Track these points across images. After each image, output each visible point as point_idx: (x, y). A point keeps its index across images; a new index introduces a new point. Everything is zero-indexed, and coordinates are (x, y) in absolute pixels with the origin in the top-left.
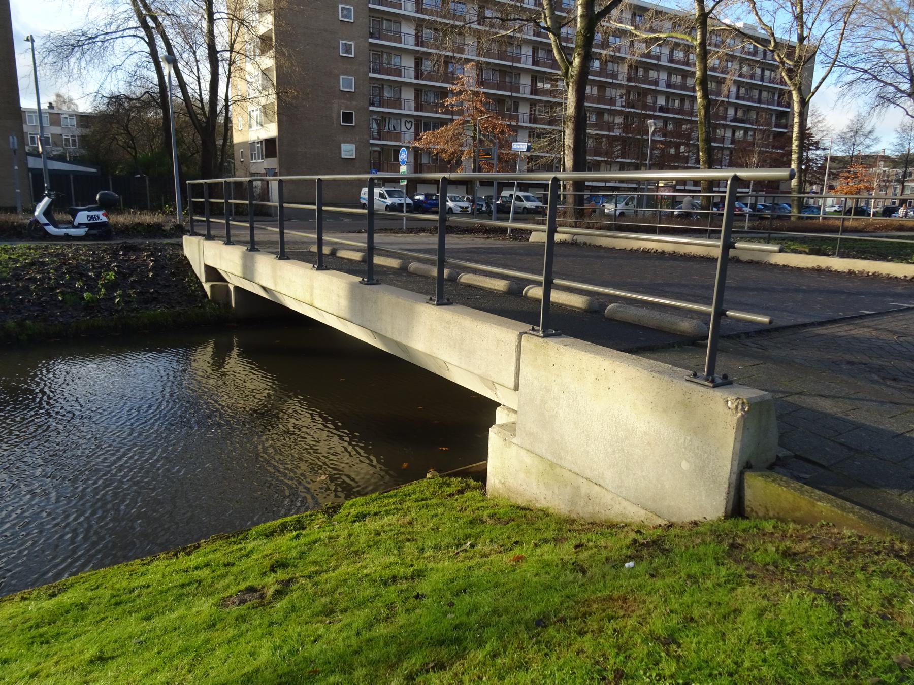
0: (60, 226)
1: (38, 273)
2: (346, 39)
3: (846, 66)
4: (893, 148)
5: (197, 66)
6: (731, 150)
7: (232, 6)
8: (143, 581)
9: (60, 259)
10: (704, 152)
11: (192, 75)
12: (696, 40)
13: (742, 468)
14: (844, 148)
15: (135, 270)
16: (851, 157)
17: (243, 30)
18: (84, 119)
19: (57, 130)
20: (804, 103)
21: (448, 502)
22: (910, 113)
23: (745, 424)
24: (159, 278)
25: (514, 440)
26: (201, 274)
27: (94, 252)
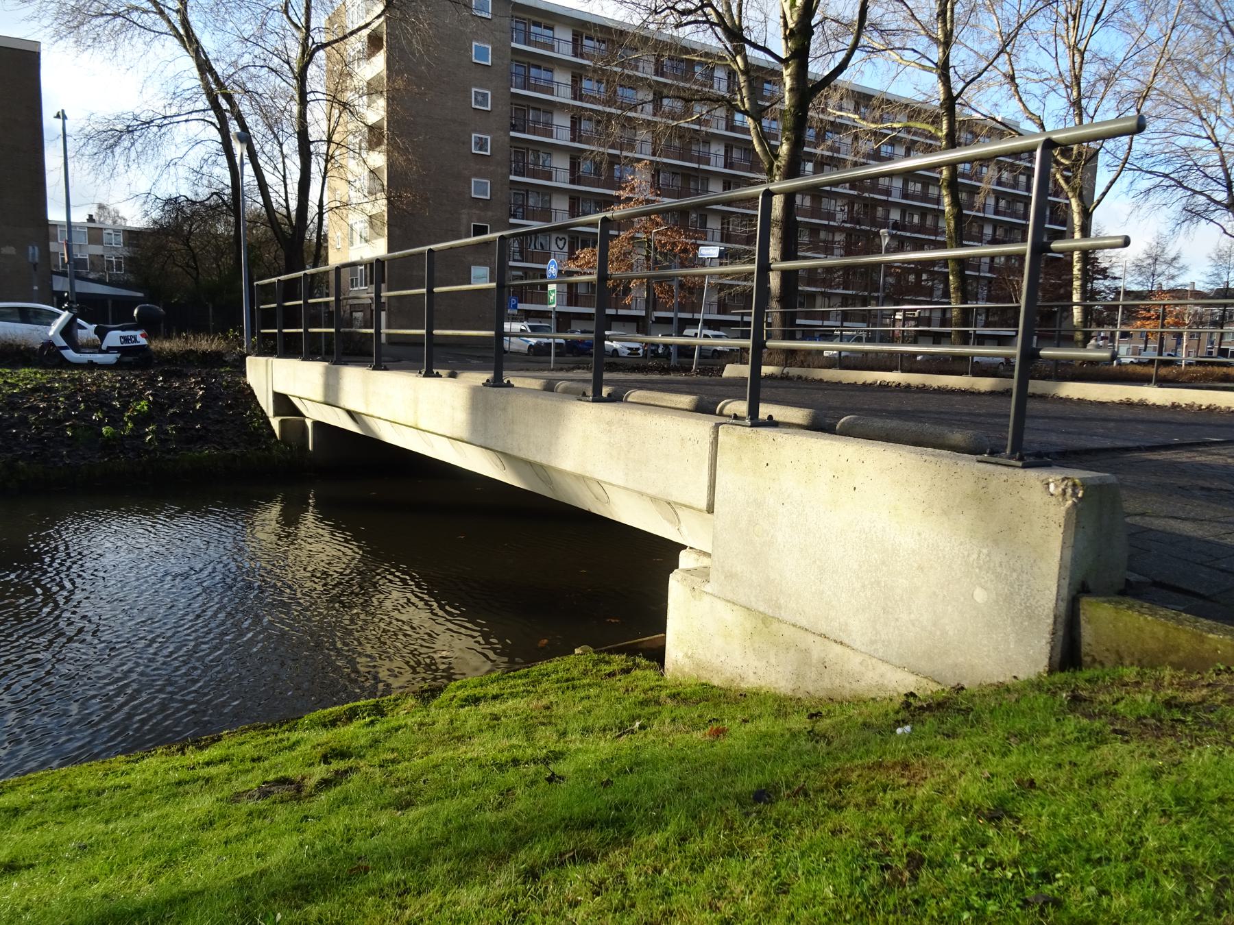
0: (83, 350)
1: (42, 400)
2: (480, 132)
3: (1140, 169)
4: (1207, 280)
5: (284, 162)
6: (990, 280)
7: (332, 87)
8: (122, 781)
9: (75, 385)
11: (277, 174)
12: (941, 131)
13: (1075, 593)
14: (1140, 279)
15: (178, 400)
17: (346, 116)
18: (133, 236)
19: (97, 250)
20: (1087, 215)
21: (607, 682)
22: (1229, 231)
24: (210, 411)
25: (708, 588)
26: (267, 404)
27: (123, 378)
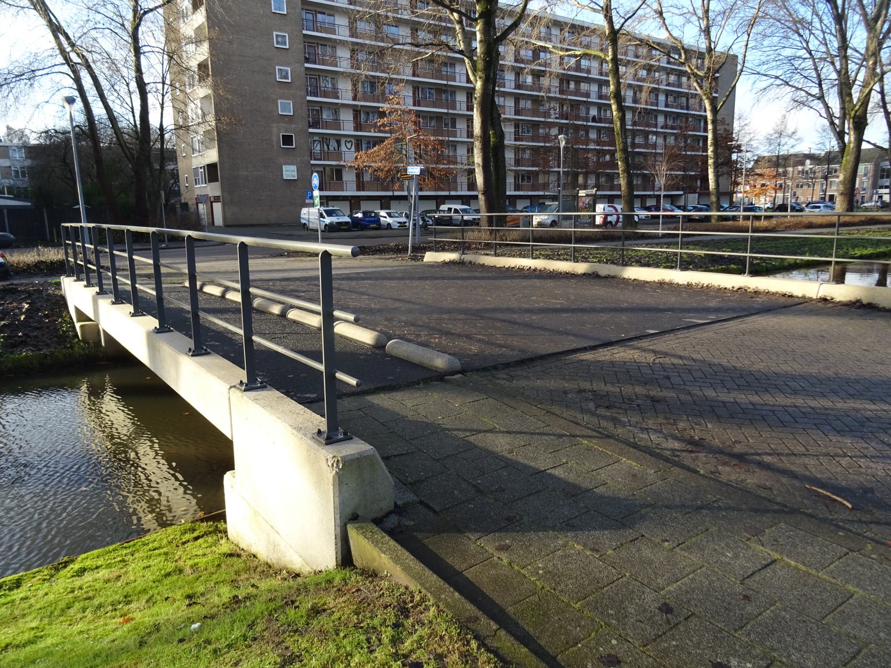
3: (758, 73)
10: (622, 161)
16: (778, 157)
18: (32, 151)
23: (341, 480)
